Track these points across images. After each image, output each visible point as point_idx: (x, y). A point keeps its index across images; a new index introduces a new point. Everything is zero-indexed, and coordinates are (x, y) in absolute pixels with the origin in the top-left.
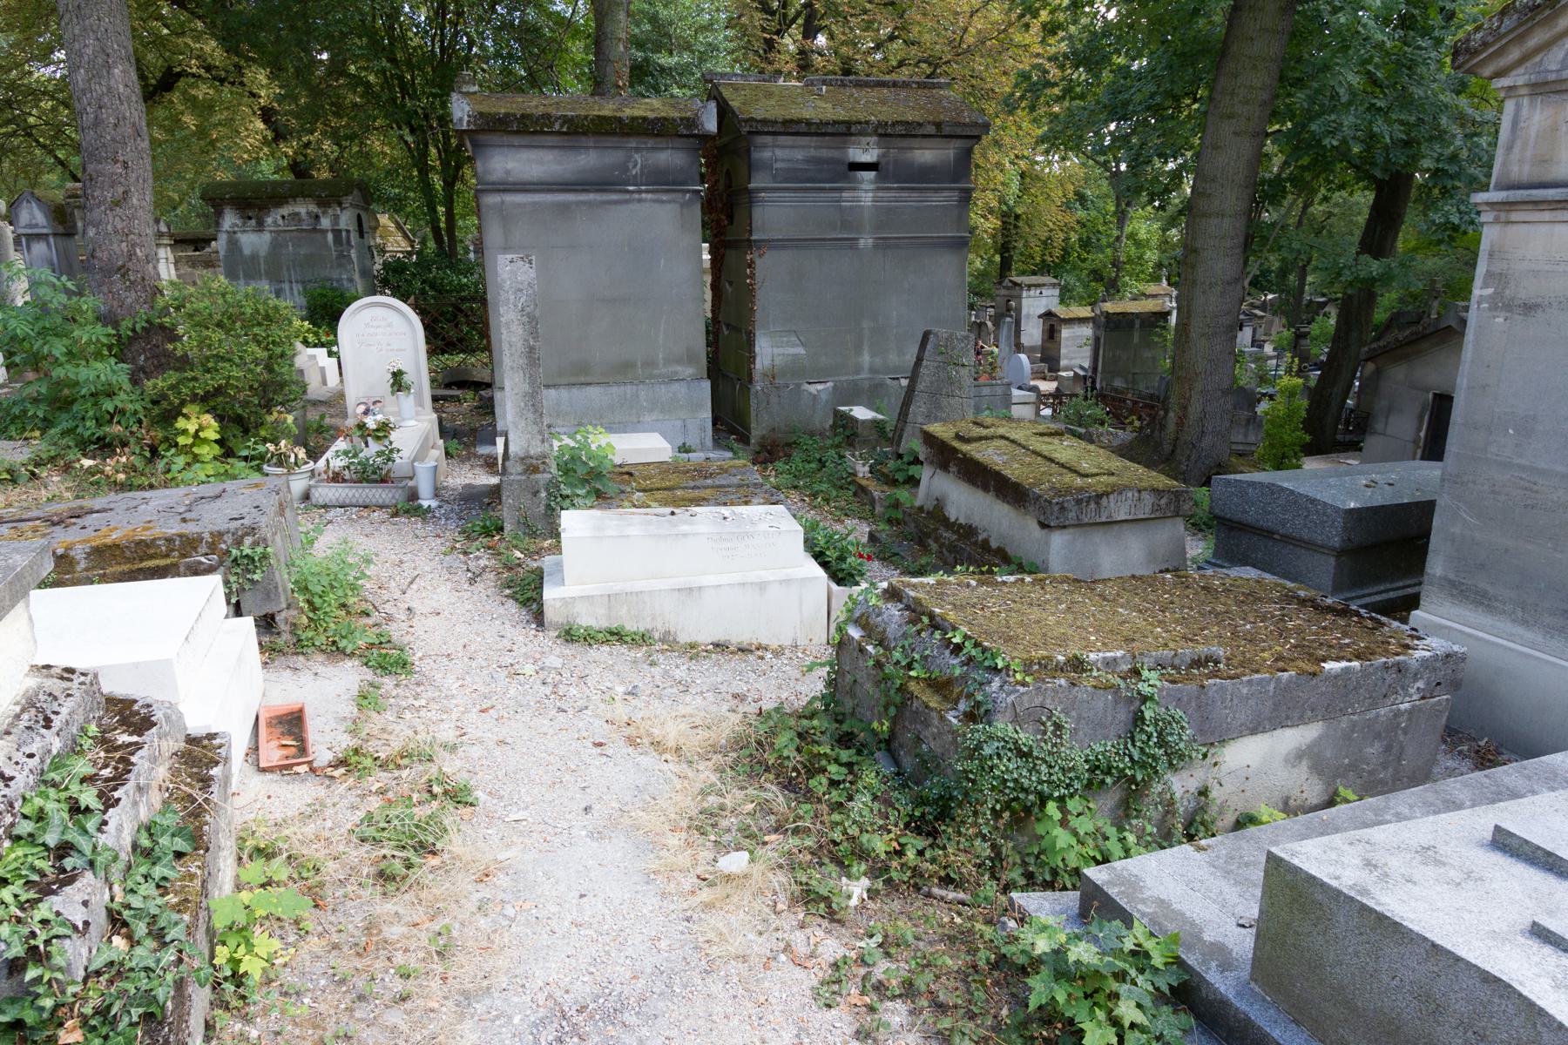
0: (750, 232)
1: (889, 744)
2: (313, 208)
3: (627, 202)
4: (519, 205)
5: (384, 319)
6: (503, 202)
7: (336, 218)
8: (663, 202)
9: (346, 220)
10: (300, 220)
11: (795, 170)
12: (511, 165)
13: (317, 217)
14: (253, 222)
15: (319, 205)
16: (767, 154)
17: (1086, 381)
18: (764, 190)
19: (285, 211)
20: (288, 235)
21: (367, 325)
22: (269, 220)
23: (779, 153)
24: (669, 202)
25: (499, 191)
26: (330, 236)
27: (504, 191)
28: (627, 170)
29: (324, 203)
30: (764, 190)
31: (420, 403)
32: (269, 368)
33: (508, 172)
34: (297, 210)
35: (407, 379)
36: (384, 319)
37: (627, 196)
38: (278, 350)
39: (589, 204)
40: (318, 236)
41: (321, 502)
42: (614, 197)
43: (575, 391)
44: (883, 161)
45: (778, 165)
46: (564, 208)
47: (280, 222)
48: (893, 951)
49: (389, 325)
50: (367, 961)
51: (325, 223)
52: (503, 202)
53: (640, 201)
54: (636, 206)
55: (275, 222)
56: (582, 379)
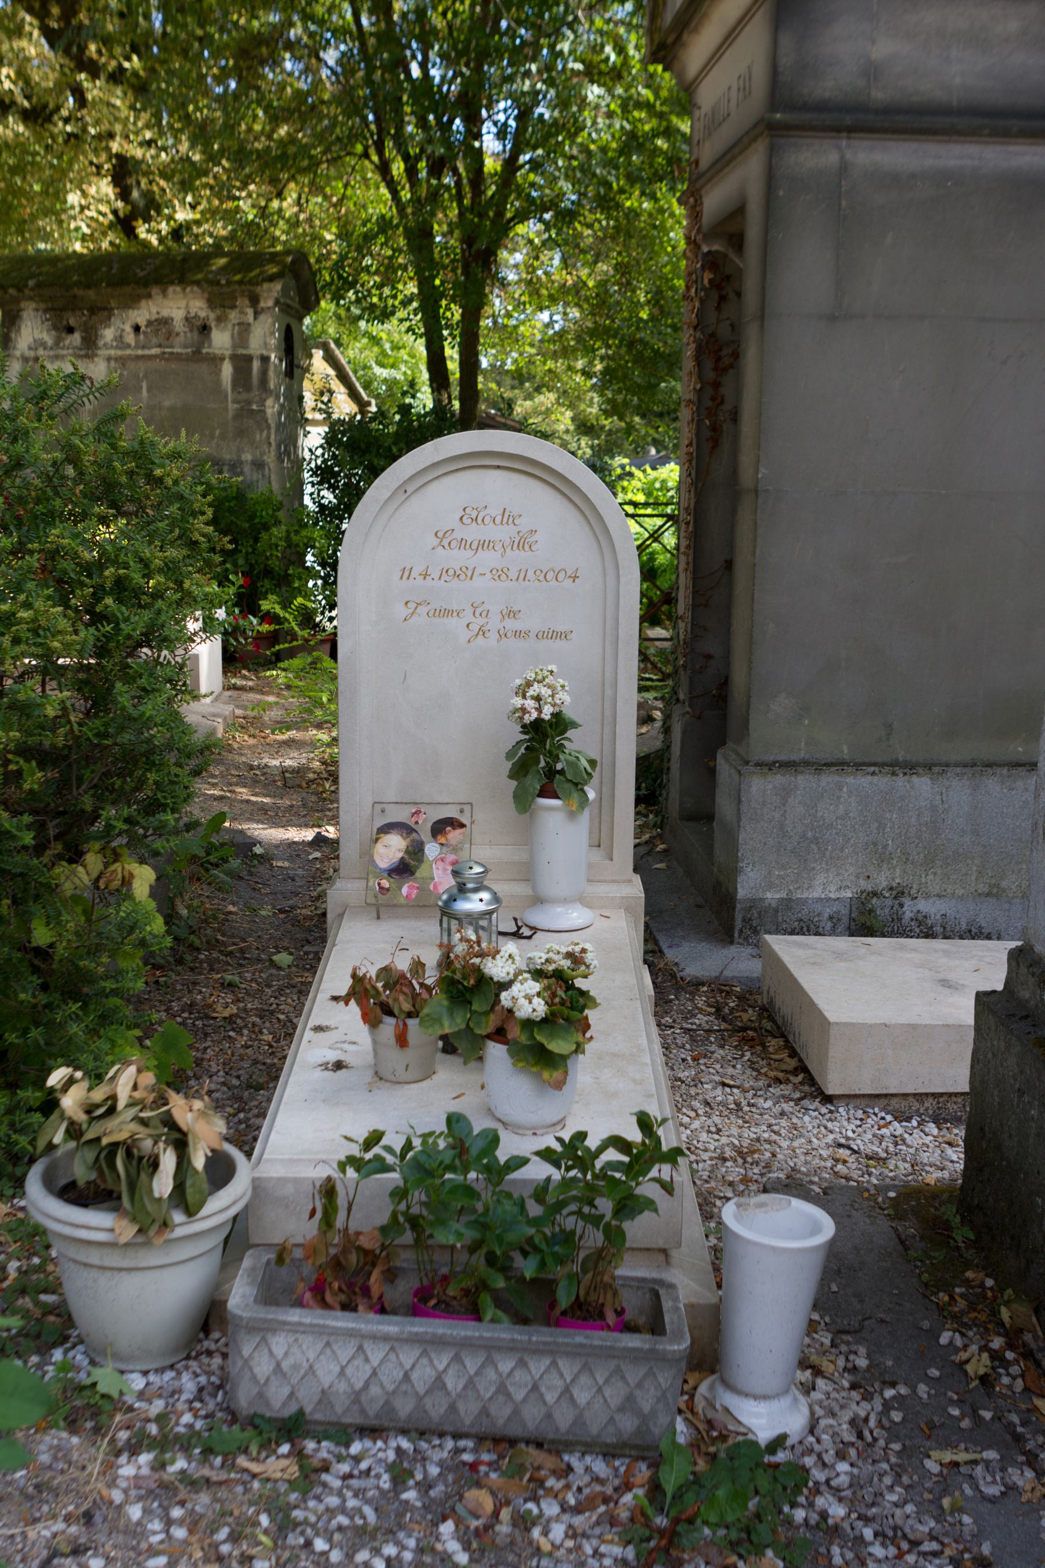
2: (198, 306)
4: (895, 180)
5: (507, 517)
6: (844, 168)
7: (244, 329)
9: (264, 337)
10: (170, 335)
13: (205, 329)
14: (76, 338)
15: (211, 304)
19: (142, 314)
20: (142, 366)
21: (443, 538)
22: (108, 334)
25: (837, 130)
26: (227, 370)
27: (852, 130)
29: (222, 301)
31: (600, 841)
32: (95, 690)
33: (872, 71)
34: (165, 313)
35: (579, 744)
36: (507, 517)
38: (137, 622)
40: (203, 369)
41: (278, 1401)
43: (993, 785)
47: (130, 338)
49: (522, 543)
51: (221, 340)
52: (844, 168)
55: (120, 338)
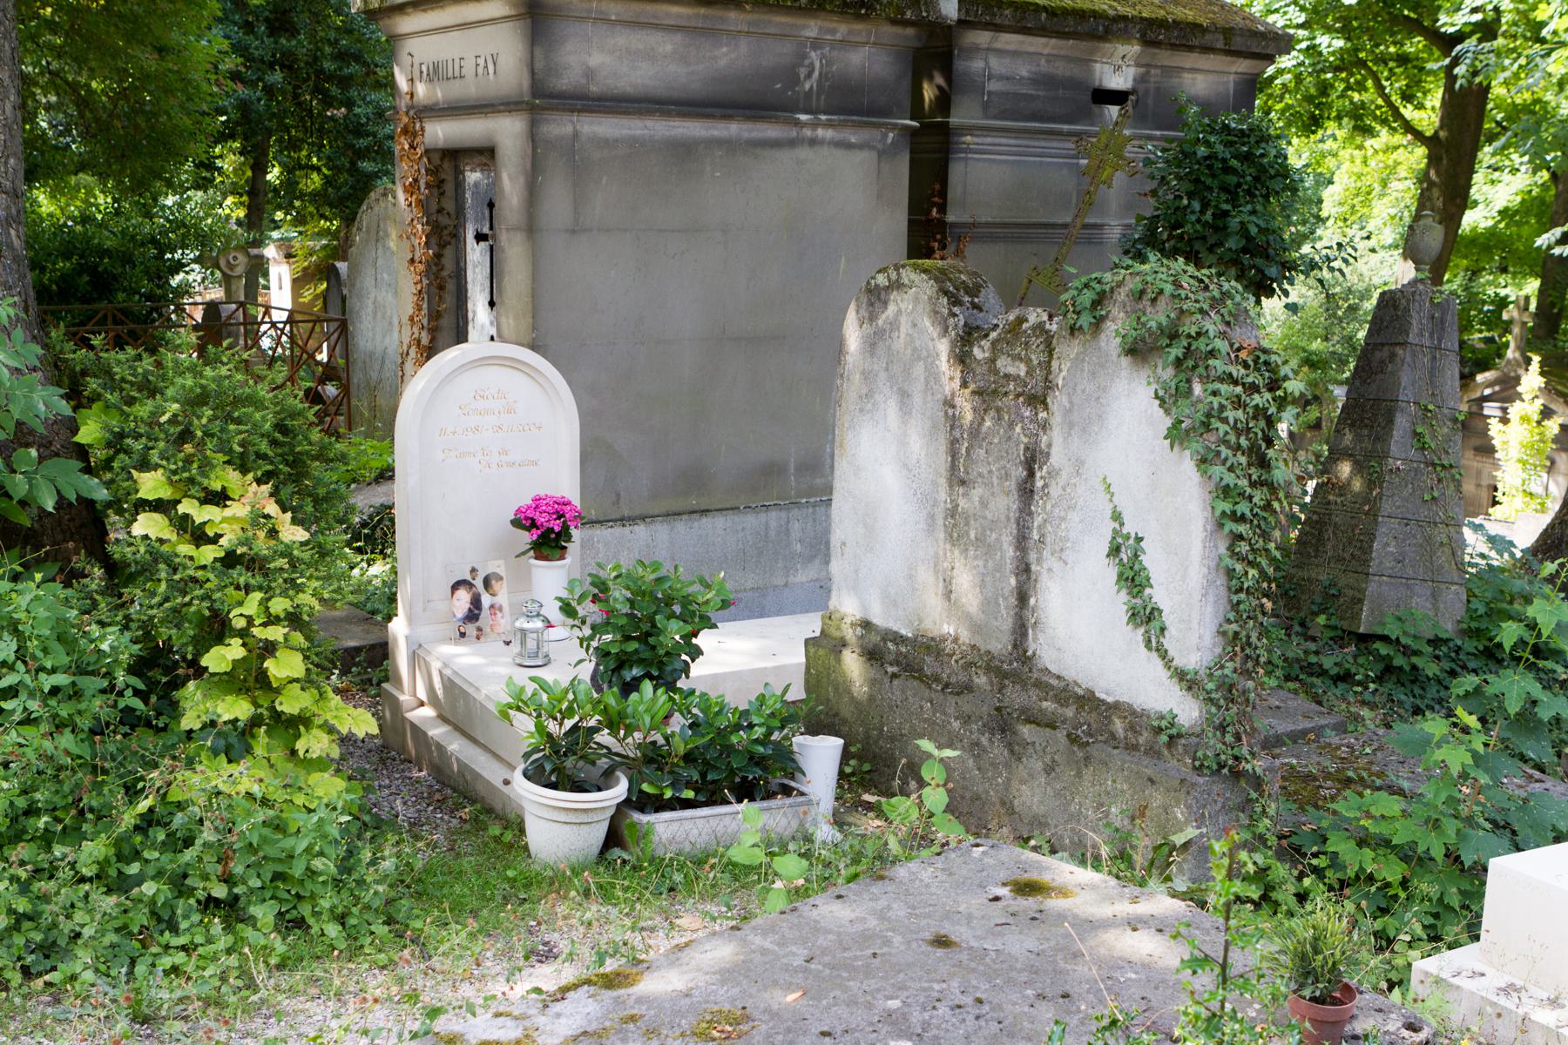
0: (943, 209)
1: (608, 623)
3: (792, 143)
4: (607, 143)
6: (576, 135)
8: (849, 146)
11: (1017, 96)
12: (596, 59)
16: (977, 65)
17: (1460, 526)
18: (971, 130)
23: (996, 64)
24: (860, 147)
28: (795, 80)
30: (971, 130)
33: (590, 74)
37: (793, 133)
39: (730, 145)
42: (771, 131)
43: (681, 526)
44: (1141, 88)
45: (993, 86)
46: (684, 151)
48: (464, 597)
50: (198, 842)
52: (576, 135)
53: (813, 142)
54: (803, 153)
56: (693, 502)
